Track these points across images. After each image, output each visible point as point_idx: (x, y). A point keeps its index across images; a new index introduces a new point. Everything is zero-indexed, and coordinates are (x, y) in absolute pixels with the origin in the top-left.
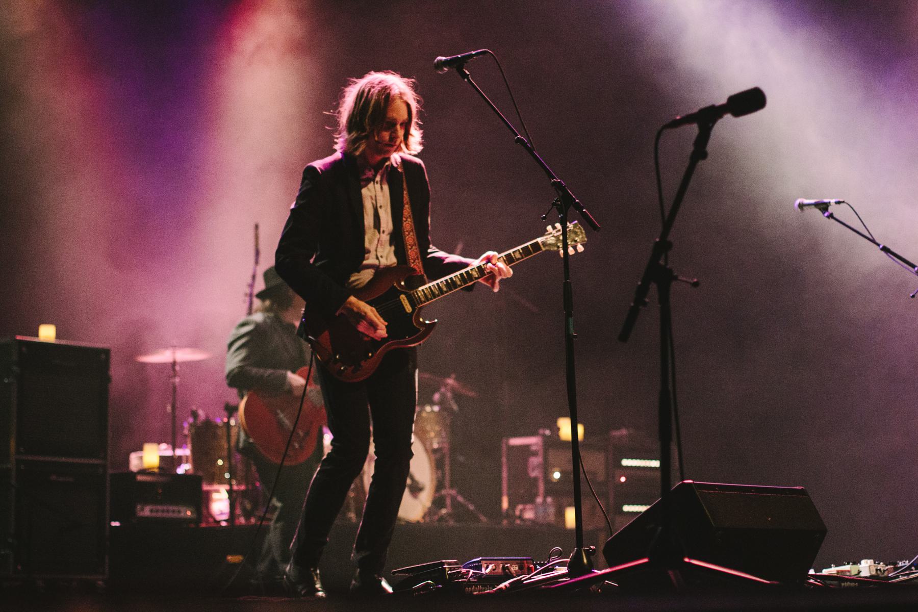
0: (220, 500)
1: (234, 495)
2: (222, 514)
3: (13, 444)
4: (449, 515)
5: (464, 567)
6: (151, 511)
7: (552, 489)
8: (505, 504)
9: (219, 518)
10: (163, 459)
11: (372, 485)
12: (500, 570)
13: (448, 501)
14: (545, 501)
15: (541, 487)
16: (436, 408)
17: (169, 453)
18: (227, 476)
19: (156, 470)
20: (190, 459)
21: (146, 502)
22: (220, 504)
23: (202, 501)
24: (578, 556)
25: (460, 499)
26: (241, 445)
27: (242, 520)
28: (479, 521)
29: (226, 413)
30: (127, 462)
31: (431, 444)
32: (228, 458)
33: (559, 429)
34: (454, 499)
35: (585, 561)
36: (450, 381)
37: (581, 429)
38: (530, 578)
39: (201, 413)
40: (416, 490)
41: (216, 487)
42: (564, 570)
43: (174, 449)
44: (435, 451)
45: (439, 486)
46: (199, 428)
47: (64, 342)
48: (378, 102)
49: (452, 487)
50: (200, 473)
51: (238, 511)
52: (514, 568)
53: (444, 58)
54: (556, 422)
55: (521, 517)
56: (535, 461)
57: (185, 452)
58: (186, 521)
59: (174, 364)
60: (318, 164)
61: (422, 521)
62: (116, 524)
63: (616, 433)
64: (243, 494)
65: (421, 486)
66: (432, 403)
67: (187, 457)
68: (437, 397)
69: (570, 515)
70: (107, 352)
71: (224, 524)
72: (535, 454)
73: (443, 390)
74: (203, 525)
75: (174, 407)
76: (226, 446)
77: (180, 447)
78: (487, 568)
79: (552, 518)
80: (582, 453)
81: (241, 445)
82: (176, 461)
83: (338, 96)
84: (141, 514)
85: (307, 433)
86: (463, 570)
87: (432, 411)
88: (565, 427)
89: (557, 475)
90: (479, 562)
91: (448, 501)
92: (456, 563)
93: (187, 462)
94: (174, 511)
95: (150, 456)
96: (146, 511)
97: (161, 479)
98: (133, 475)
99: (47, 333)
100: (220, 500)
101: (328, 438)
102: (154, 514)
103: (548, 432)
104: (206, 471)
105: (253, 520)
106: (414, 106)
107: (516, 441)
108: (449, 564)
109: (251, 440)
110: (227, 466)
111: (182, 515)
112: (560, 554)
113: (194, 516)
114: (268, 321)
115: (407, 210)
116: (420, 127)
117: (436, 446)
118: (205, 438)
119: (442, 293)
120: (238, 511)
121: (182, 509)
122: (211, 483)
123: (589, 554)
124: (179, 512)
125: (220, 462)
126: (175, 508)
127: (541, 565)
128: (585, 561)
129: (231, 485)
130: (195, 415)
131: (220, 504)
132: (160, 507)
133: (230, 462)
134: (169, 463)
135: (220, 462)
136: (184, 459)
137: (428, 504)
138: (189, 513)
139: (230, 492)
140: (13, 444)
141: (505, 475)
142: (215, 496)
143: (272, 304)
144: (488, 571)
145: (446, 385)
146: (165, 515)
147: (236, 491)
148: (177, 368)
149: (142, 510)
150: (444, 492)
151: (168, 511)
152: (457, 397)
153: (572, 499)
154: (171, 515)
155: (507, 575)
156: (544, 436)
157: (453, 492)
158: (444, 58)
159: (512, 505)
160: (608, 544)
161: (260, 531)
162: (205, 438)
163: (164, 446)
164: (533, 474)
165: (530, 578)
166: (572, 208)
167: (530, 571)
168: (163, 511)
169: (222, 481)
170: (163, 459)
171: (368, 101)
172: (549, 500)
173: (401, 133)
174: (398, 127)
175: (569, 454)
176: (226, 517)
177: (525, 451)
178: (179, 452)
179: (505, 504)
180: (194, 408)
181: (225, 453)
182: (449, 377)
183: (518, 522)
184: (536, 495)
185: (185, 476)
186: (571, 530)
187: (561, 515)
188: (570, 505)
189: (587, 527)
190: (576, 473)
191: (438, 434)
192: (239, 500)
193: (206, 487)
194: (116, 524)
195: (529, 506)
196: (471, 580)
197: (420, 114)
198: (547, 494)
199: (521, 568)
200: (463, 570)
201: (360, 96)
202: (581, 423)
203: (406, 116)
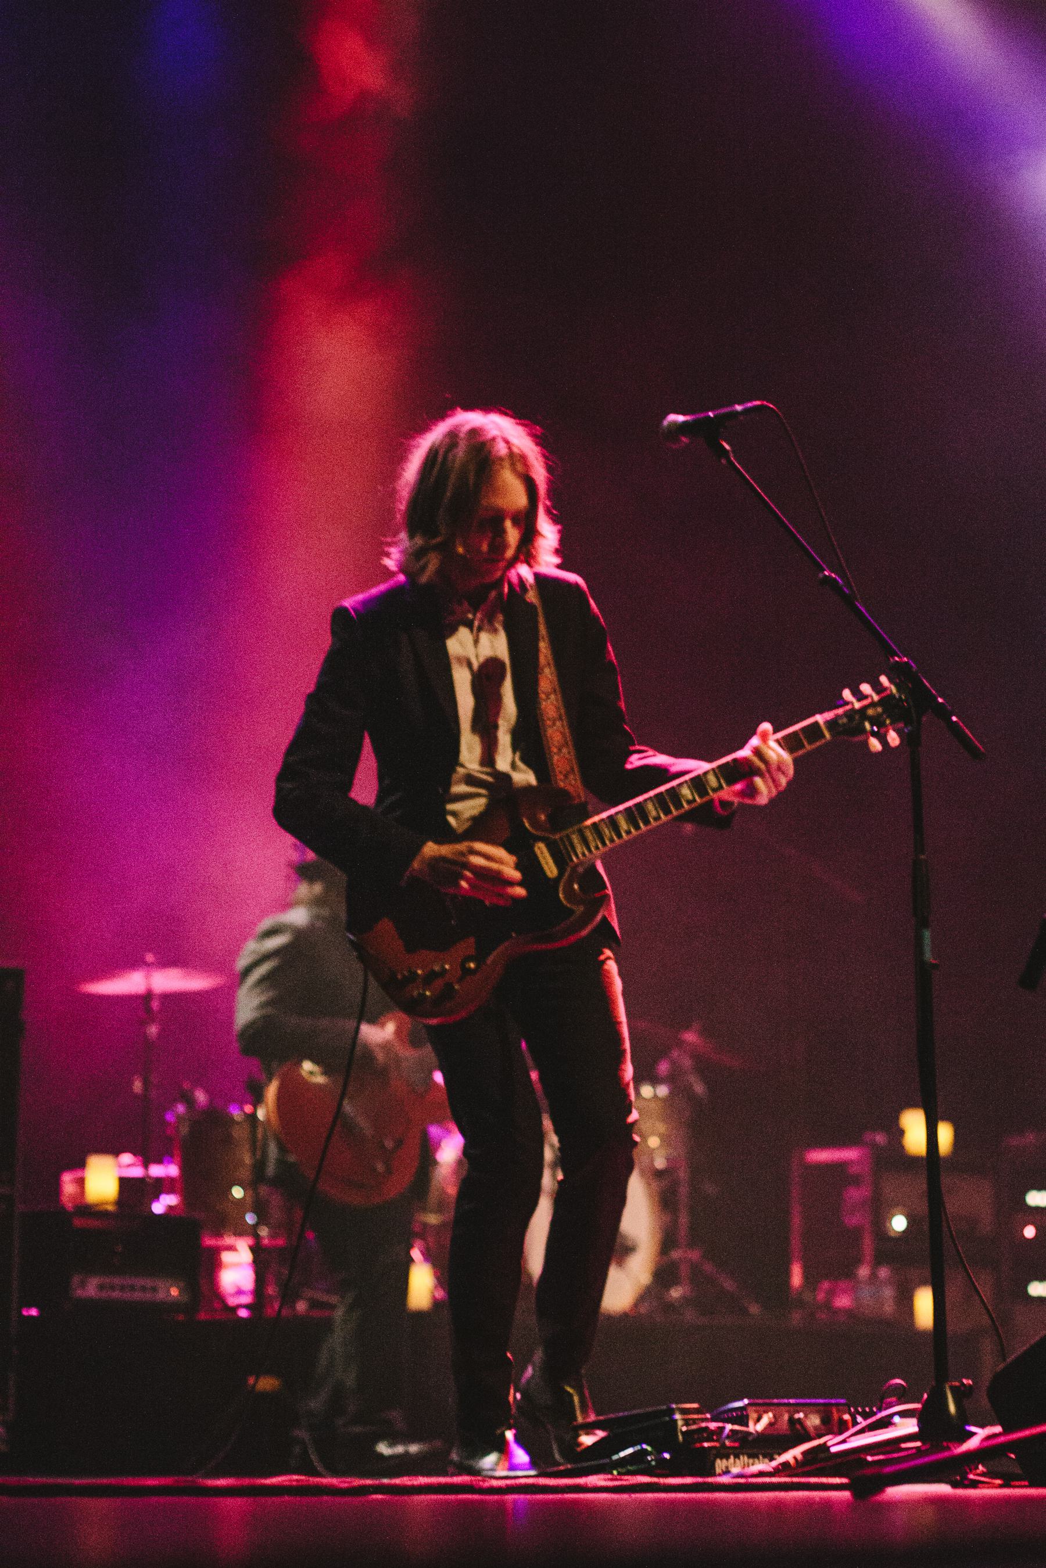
0: (236, 1265)
2: (240, 1292)
4: (685, 1300)
5: (712, 1420)
6: (101, 1287)
7: (890, 1249)
8: (797, 1278)
9: (232, 1301)
10: (124, 1183)
13: (684, 1271)
14: (873, 1276)
15: (868, 1243)
16: (663, 1091)
17: (137, 1172)
18: (250, 1219)
22: (236, 1272)
24: (936, 1403)
25: (708, 1268)
26: (271, 1170)
28: (744, 1311)
31: (652, 1160)
32: (256, 1180)
33: (902, 1133)
35: (952, 1408)
36: (690, 1037)
38: (844, 1441)
41: (229, 1240)
42: (909, 1426)
44: (659, 1174)
49: (691, 1245)
52: (814, 1421)
53: (681, 418)
54: (896, 1119)
55: (828, 1305)
56: (855, 1195)
58: (173, 1307)
60: (347, 603)
63: (1015, 1141)
65: (630, 1243)
66: (655, 1081)
68: (663, 1068)
69: (924, 1303)
71: (243, 1313)
72: (856, 1181)
73: (675, 1054)
74: (202, 1316)
76: (247, 1159)
77: (159, 1162)
78: (758, 1420)
79: (889, 1308)
80: (946, 1180)
81: (271, 1170)
83: (400, 457)
84: (79, 1293)
85: (399, 1143)
86: (713, 1425)
87: (655, 1096)
89: (899, 1223)
91: (684, 1271)
94: (144, 1289)
95: (102, 1180)
100: (236, 1265)
101: (450, 1151)
103: (880, 1138)
106: (540, 474)
107: (821, 1156)
108: (684, 1411)
109: (292, 1158)
110: (249, 1200)
111: (161, 1295)
113: (185, 1299)
114: (319, 924)
116: (555, 520)
117: (660, 1163)
121: (160, 1284)
123: (961, 1395)
124: (154, 1289)
125: (238, 1192)
126: (148, 1282)
127: (866, 1416)
128: (952, 1408)
131: (236, 1272)
132: (117, 1281)
135: (238, 1192)
138: (174, 1292)
141: (797, 1221)
142: (227, 1257)
143: (327, 890)
145: (680, 1044)
146: (127, 1295)
147: (267, 1247)
149: (83, 1285)
150: (676, 1254)
151: (132, 1288)
152: (703, 1067)
153: (927, 1273)
154: (138, 1296)
155: (797, 1434)
156: (874, 1145)
157: (694, 1255)
158: (681, 418)
160: (997, 1378)
161: (315, 1330)
163: (127, 1158)
164: (854, 1220)
169: (241, 1231)
172: (884, 1273)
173: (513, 535)
174: (508, 524)
178: (157, 1171)
179: (797, 1278)
181: (245, 1173)
182: (688, 1027)
183: (822, 1316)
184: (858, 1261)
186: (923, 1334)
188: (923, 1283)
190: (932, 1221)
191: (665, 1139)
193: (210, 1242)
195: (843, 1284)
197: (551, 493)
198: (879, 1260)
199: (826, 1420)
200: (713, 1425)
201: (432, 455)
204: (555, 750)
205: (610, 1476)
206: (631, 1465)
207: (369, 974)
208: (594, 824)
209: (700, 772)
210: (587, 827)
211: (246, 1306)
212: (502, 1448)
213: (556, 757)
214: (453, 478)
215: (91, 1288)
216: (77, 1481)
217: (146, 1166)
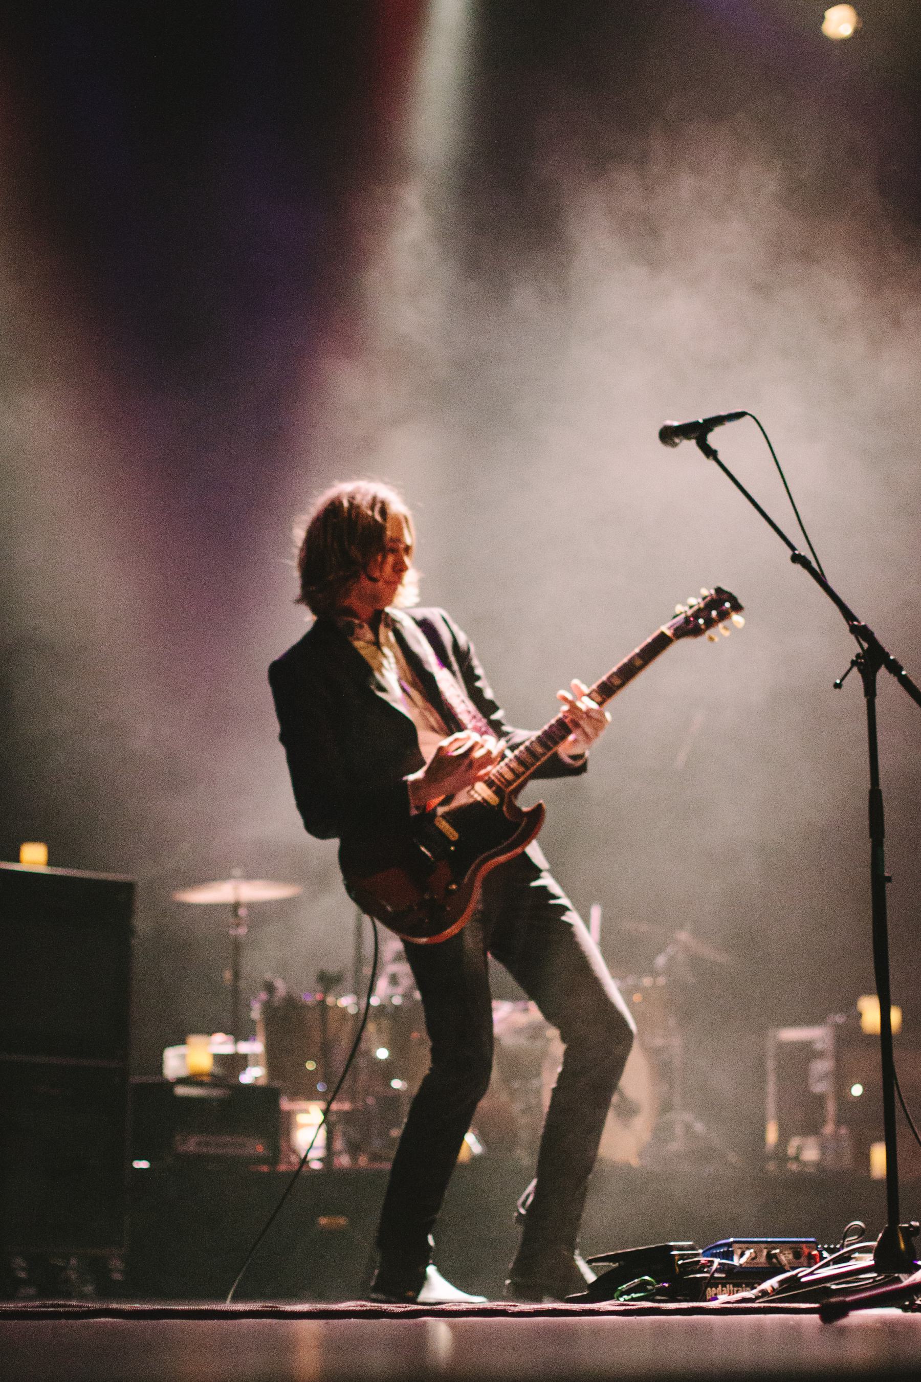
1: (333, 1118)
6: (199, 1144)
11: (555, 1091)
12: (762, 1259)
15: (831, 1108)
18: (320, 1087)
19: (206, 1079)
20: (263, 1060)
23: (277, 1127)
27: (344, 1161)
29: (319, 988)
30: (158, 1065)
33: (860, 1015)
34: (688, 1128)
35: (902, 1246)
37: (895, 1016)
38: (811, 1273)
39: (281, 987)
40: (629, 1111)
41: (301, 1104)
42: (868, 1260)
45: (665, 1107)
46: (276, 1009)
47: (59, 871)
50: (277, 1084)
51: (339, 1145)
52: (785, 1258)
55: (797, 1158)
57: (254, 1047)
59: (236, 906)
61: (635, 1162)
62: (142, 1164)
64: (348, 1117)
67: (256, 1055)
69: (879, 1156)
70: (128, 888)
71: (316, 1165)
72: (820, 1055)
75: (236, 975)
77: (246, 1039)
78: (742, 1255)
79: (847, 1161)
82: (236, 1062)
84: (182, 1149)
88: (870, 1012)
90: (729, 1245)
92: (692, 1248)
93: (256, 1064)
95: (191, 1058)
97: (216, 1093)
98: (168, 1086)
99: (34, 857)
104: (286, 1079)
105: (363, 1160)
111: (248, 1151)
112: (863, 1234)
118: (289, 1026)
120: (339, 1145)
122: (295, 1095)
127: (831, 1251)
128: (902, 1246)
130: (270, 988)
134: (233, 1063)
135: (311, 1066)
136: (250, 1059)
137: (646, 1137)
139: (326, 1112)
142: (301, 1118)
144: (743, 1260)
148: (242, 912)
150: (671, 1116)
153: (881, 1130)
155: (774, 1269)
157: (688, 1117)
159: (784, 1137)
162: (289, 1026)
163: (219, 1037)
165: (811, 1273)
167: (811, 1260)
169: (311, 1095)
170: (220, 1059)
175: (876, 1056)
177: (805, 1053)
178: (244, 1048)
180: (268, 976)
183: (794, 1167)
184: (823, 1122)
185: (251, 1089)
186: (878, 1182)
187: (864, 1158)
188: (877, 1140)
189: (904, 1177)
192: (340, 1128)
194: (142, 1164)
196: (716, 1275)
199: (797, 1255)
200: (703, 1260)
202: (896, 1004)
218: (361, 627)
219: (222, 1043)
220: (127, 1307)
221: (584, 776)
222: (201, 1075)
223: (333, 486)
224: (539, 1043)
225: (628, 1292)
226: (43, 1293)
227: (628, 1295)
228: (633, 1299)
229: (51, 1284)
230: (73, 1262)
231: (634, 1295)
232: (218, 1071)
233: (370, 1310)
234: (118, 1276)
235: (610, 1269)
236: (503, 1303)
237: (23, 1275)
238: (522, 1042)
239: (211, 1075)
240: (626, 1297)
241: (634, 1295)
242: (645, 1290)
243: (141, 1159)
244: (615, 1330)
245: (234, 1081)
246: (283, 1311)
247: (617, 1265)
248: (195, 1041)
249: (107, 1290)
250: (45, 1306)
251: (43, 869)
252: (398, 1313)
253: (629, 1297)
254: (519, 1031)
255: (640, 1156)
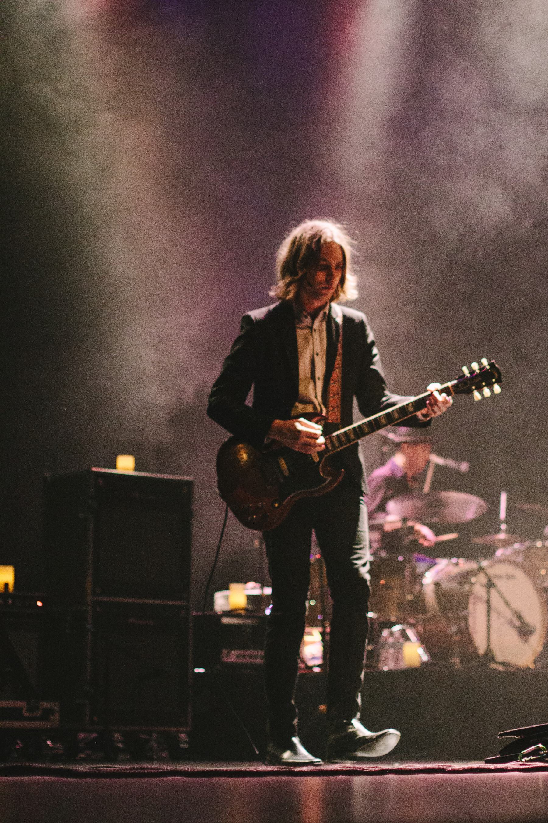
2: (314, 658)
3: (89, 585)
6: (238, 656)
9: (310, 663)
10: (251, 599)
17: (257, 592)
18: (319, 617)
19: (242, 612)
21: (232, 647)
30: (211, 602)
43: (262, 588)
47: (143, 474)
48: (309, 247)
61: (532, 666)
65: (531, 628)
70: (189, 484)
71: (317, 670)
84: (226, 660)
96: (232, 657)
97: (248, 622)
98: (217, 618)
102: (241, 660)
110: (319, 606)
115: (339, 360)
116: (356, 272)
119: (342, 445)
129: (324, 627)
133: (323, 603)
137: (539, 649)
139: (323, 634)
140: (89, 585)
149: (228, 655)
163: (251, 584)
166: (226, 435)
168: (250, 657)
170: (251, 599)
171: (299, 248)
176: (319, 662)
181: (317, 592)
203: (341, 258)
204: (332, 395)
205: (521, 763)
206: (533, 756)
207: (229, 509)
208: (337, 435)
209: (404, 404)
210: (333, 437)
211: (319, 666)
212: (293, 748)
213: (331, 399)
214: (304, 247)
215: (232, 657)
216: (56, 767)
217: (262, 588)
218: (306, 317)
219: (254, 588)
220: (188, 768)
221: (428, 428)
222: (237, 610)
223: (305, 222)
224: (467, 587)
225: (527, 755)
226: (135, 758)
227: (528, 757)
228: (531, 761)
229: (139, 751)
230: (155, 736)
231: (532, 758)
232: (250, 607)
233: (353, 770)
234: (183, 746)
235: (512, 741)
236: (442, 764)
237: (120, 745)
238: (454, 585)
239: (246, 610)
240: (527, 759)
241: (532, 758)
242: (538, 754)
243: (199, 667)
244: (520, 783)
245: (260, 614)
246: (294, 771)
247: (519, 737)
248: (235, 587)
249: (177, 756)
250: (134, 769)
251: (131, 472)
252: (371, 772)
253: (529, 759)
254: (452, 578)
255: (535, 662)
